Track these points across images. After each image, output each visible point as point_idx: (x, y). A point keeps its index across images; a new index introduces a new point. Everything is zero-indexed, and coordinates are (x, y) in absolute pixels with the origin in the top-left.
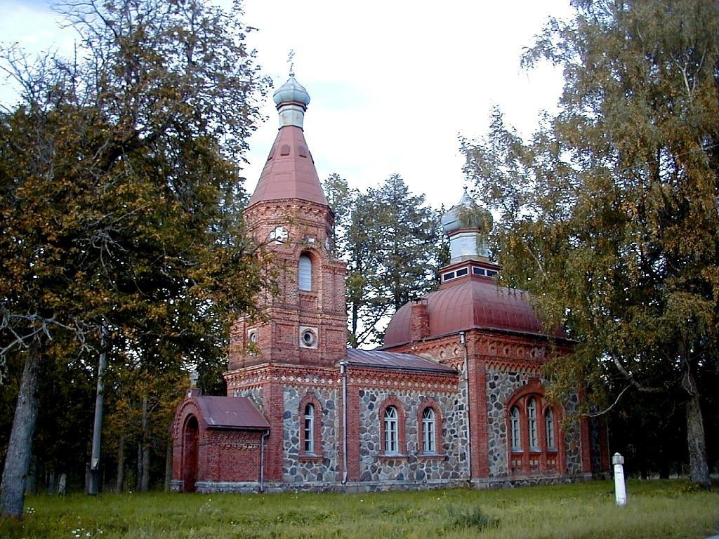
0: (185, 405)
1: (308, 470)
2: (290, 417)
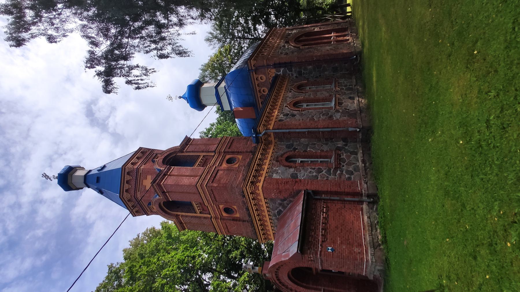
0: (280, 283)
1: (347, 161)
2: (296, 174)
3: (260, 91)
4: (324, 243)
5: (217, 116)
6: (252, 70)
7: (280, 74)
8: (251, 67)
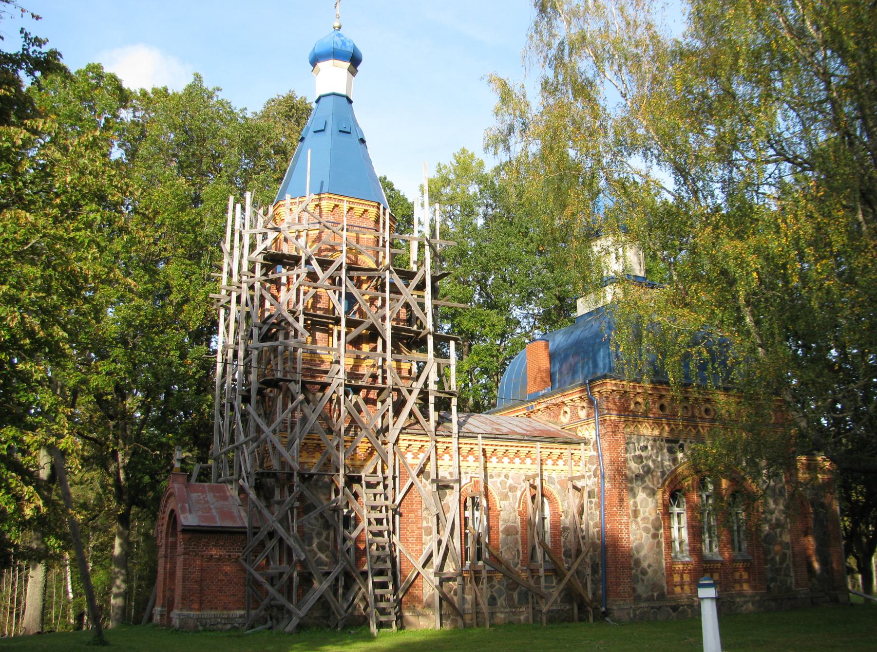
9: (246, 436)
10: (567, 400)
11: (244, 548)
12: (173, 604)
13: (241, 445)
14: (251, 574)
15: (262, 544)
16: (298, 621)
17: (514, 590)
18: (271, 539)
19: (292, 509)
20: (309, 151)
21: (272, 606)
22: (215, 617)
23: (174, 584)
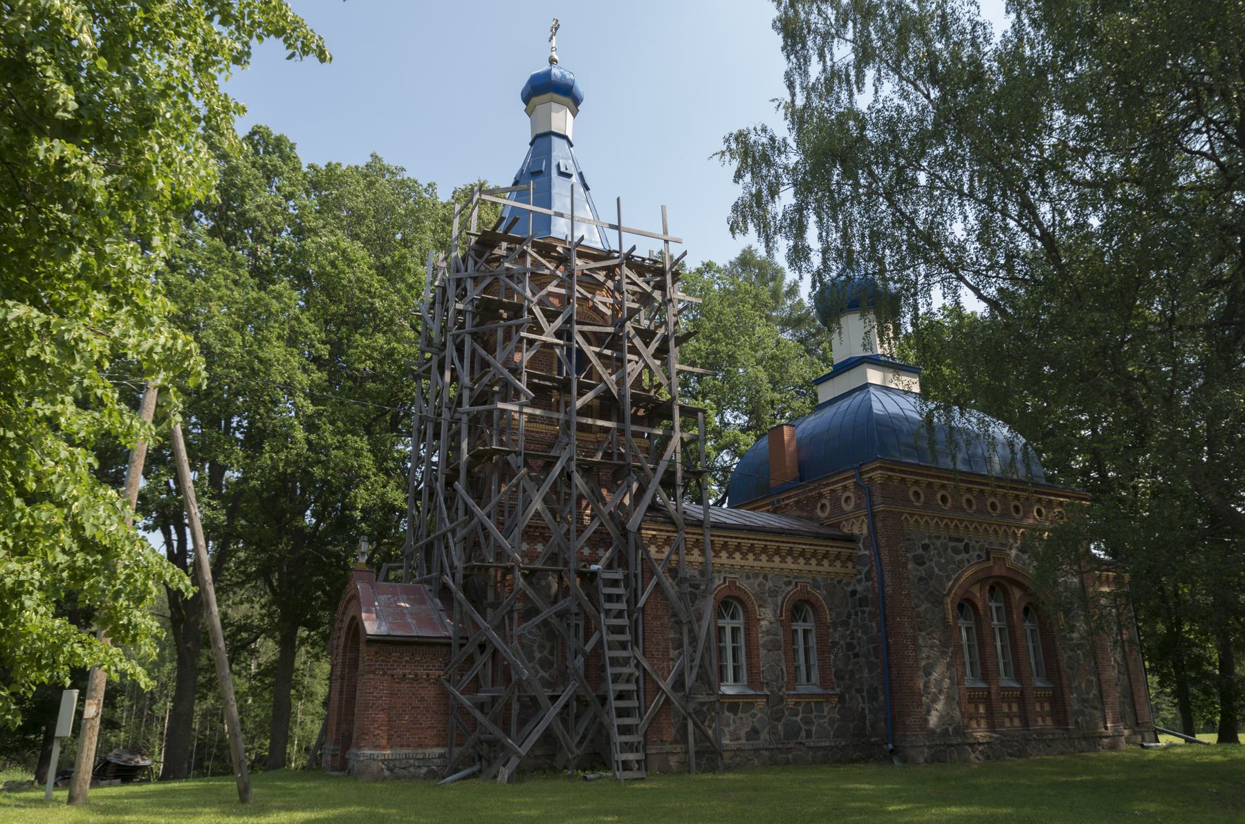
3: (845, 488)
4: (390, 678)
5: (968, 312)
6: (861, 474)
7: (860, 549)
8: (867, 472)
9: (451, 521)
10: (826, 491)
11: (446, 665)
12: (351, 738)
13: (444, 536)
14: (455, 698)
15: (471, 660)
16: (518, 761)
17: (779, 720)
18: (482, 653)
19: (510, 613)
20: (172, 527)
21: (481, 742)
22: (407, 758)
23: (353, 714)
